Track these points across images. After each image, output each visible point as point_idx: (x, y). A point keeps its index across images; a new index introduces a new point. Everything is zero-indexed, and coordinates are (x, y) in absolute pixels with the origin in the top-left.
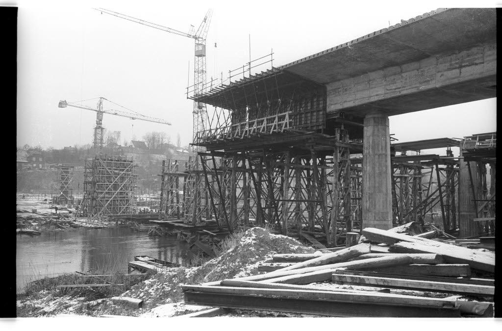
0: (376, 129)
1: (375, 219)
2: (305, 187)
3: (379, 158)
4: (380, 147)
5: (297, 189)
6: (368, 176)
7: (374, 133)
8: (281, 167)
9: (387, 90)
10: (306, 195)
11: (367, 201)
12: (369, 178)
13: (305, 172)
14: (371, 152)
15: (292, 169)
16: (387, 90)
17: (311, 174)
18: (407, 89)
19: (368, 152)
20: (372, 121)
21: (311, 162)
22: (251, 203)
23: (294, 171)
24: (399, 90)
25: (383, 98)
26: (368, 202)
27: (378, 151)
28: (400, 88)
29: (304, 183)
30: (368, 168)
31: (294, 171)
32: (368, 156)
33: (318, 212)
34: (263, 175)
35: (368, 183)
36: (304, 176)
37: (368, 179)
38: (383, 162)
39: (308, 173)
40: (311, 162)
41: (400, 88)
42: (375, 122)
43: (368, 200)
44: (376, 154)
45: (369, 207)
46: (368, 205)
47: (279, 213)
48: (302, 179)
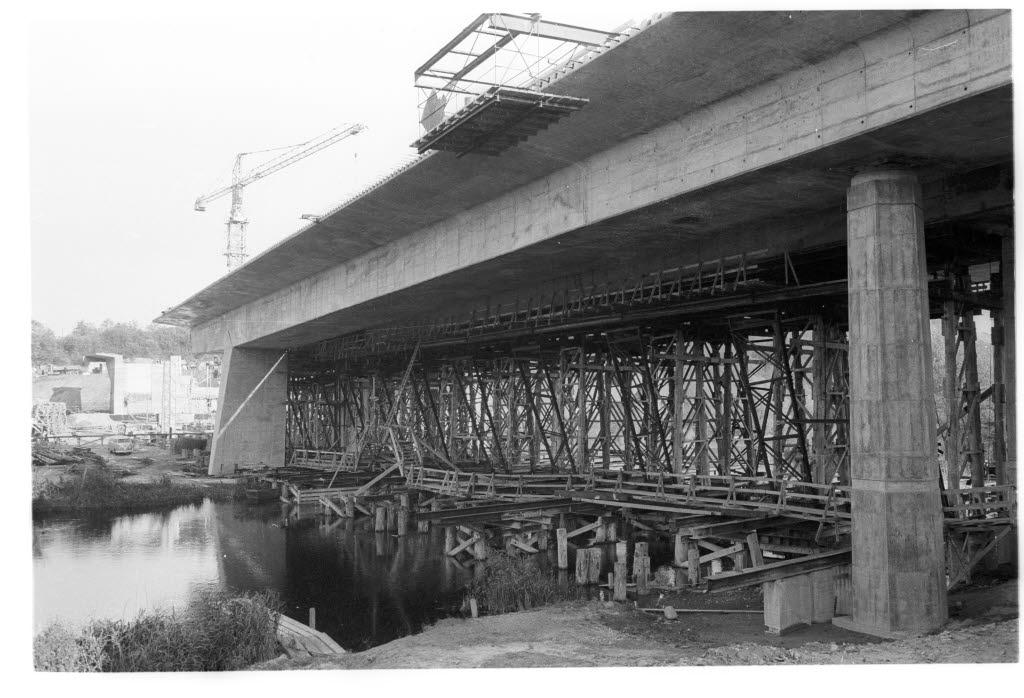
0: (885, 215)
1: (889, 476)
2: (710, 396)
3: (896, 299)
4: (900, 268)
5: (699, 405)
6: (864, 351)
7: (879, 226)
8: (668, 364)
9: (923, 86)
10: (713, 411)
11: (863, 427)
12: (869, 358)
13: (711, 368)
14: (871, 281)
15: (691, 364)
16: (923, 86)
17: (721, 374)
18: (988, 75)
19: (861, 282)
20: (871, 195)
21: (722, 350)
22: (614, 428)
23: (693, 367)
24: (963, 80)
25: (911, 112)
26: (867, 427)
27: (894, 278)
28: (965, 74)
29: (708, 388)
30: (864, 329)
31: (693, 367)
32: (863, 294)
33: (736, 442)
34: (635, 377)
35: (865, 372)
36: (708, 378)
37: (864, 361)
38: (908, 309)
39: (716, 371)
40: (722, 350)
41: (965, 74)
42: (880, 194)
43: (866, 420)
44: (888, 288)
45: (871, 443)
46: (867, 434)
47: (668, 443)
48: (705, 384)
